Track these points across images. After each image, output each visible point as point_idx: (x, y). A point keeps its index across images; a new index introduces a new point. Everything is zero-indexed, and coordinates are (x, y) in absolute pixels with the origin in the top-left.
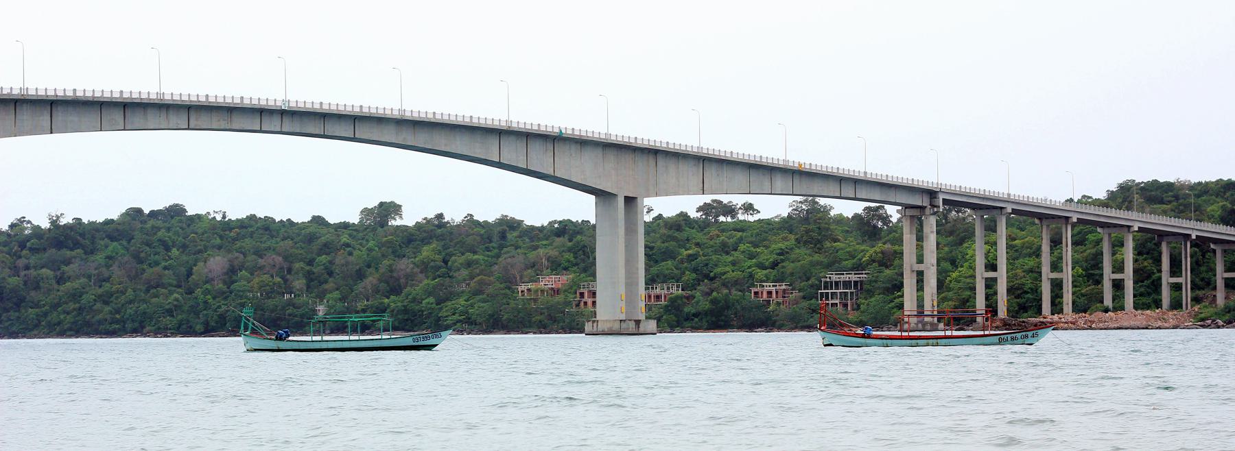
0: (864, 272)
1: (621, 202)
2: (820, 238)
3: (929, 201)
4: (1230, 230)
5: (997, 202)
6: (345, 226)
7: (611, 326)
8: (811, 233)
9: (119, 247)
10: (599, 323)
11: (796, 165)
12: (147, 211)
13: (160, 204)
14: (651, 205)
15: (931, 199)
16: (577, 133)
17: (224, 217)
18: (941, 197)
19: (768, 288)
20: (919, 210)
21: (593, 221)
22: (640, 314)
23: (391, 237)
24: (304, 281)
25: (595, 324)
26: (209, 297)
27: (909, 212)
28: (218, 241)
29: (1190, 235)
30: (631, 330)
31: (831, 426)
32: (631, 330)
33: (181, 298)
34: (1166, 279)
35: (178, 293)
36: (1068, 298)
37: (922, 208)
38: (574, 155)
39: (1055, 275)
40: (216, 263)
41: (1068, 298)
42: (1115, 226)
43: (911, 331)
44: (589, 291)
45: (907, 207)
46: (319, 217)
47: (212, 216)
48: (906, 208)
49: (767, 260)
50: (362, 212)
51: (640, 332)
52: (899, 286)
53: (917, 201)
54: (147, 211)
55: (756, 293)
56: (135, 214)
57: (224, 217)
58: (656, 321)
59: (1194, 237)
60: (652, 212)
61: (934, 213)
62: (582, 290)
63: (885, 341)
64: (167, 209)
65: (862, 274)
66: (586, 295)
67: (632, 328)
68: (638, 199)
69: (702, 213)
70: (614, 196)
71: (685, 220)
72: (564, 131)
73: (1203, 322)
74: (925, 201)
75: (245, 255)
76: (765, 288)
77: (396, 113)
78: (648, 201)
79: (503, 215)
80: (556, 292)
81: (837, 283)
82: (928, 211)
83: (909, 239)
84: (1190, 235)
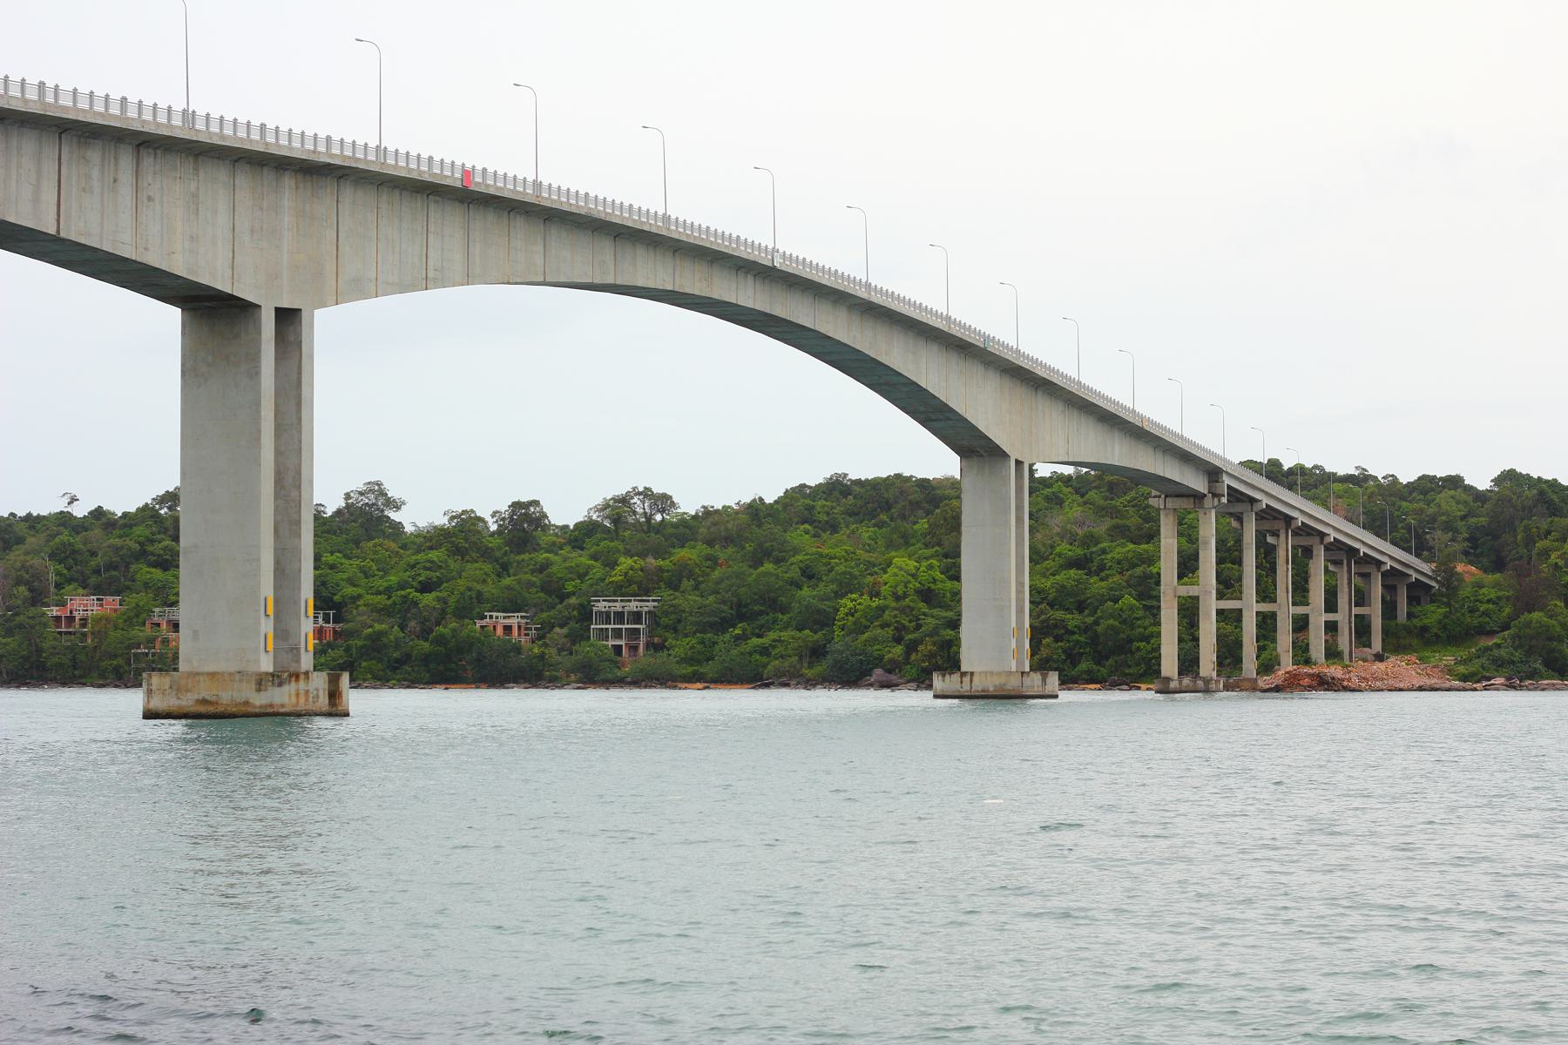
0: (650, 598)
2: (467, 546)
5: (1257, 492)
7: (1003, 681)
8: (454, 539)
10: (976, 678)
14: (74, 493)
20: (1192, 500)
21: (958, 476)
25: (967, 679)
30: (1036, 689)
31: (1554, 916)
32: (1036, 689)
37: (1197, 497)
39: (1266, 607)
43: (1129, 702)
44: (169, 622)
48: (1166, 497)
51: (1047, 693)
58: (1057, 672)
60: (75, 503)
62: (156, 619)
65: (648, 601)
67: (1038, 686)
71: (152, 517)
74: (1198, 484)
81: (608, 614)
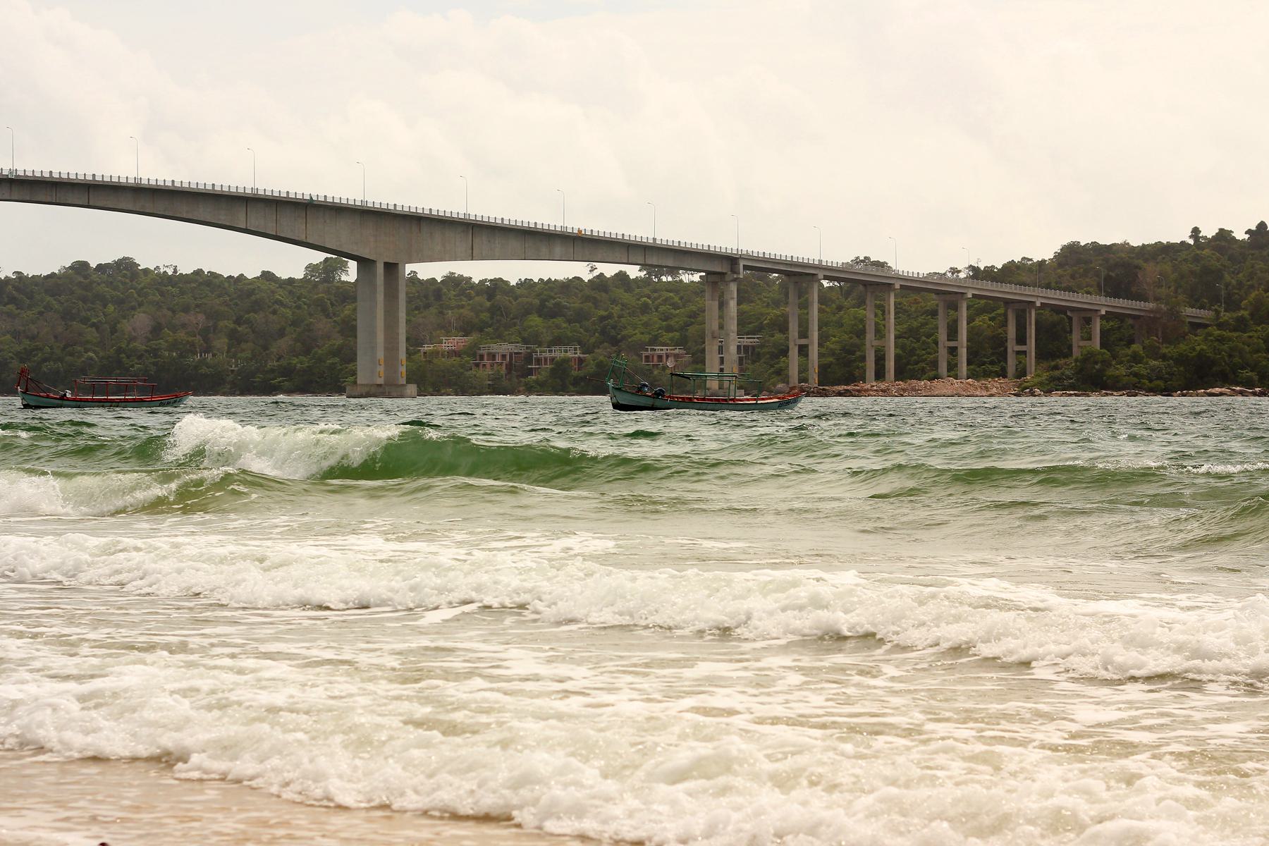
1: (380, 269)
3: (729, 266)
4: (1060, 295)
6: (291, 281)
9: (54, 302)
11: (576, 231)
12: (93, 265)
13: (108, 257)
15: (732, 265)
16: (329, 200)
17: (175, 271)
18: (742, 263)
19: (659, 352)
22: (400, 379)
23: (323, 295)
24: (226, 340)
26: (123, 355)
27: (711, 278)
28: (158, 298)
29: (1034, 302)
33: (95, 357)
34: (1012, 346)
35: (95, 352)
36: (890, 365)
38: (328, 221)
40: (140, 321)
41: (890, 365)
42: (950, 293)
45: (708, 273)
46: (268, 272)
47: (162, 271)
49: (677, 322)
50: (306, 268)
52: (785, 352)
53: (717, 268)
54: (93, 265)
55: (647, 357)
56: (80, 268)
57: (175, 271)
59: (1038, 304)
61: (735, 280)
63: (79, 403)
64: (116, 263)
66: (486, 357)
68: (400, 265)
69: (645, 272)
70: (374, 262)
72: (315, 198)
73: (1054, 385)
75: (174, 312)
76: (657, 352)
77: (131, 181)
78: (409, 268)
79: (450, 273)
80: (456, 353)
82: (728, 278)
83: (712, 305)
84: (1034, 302)
